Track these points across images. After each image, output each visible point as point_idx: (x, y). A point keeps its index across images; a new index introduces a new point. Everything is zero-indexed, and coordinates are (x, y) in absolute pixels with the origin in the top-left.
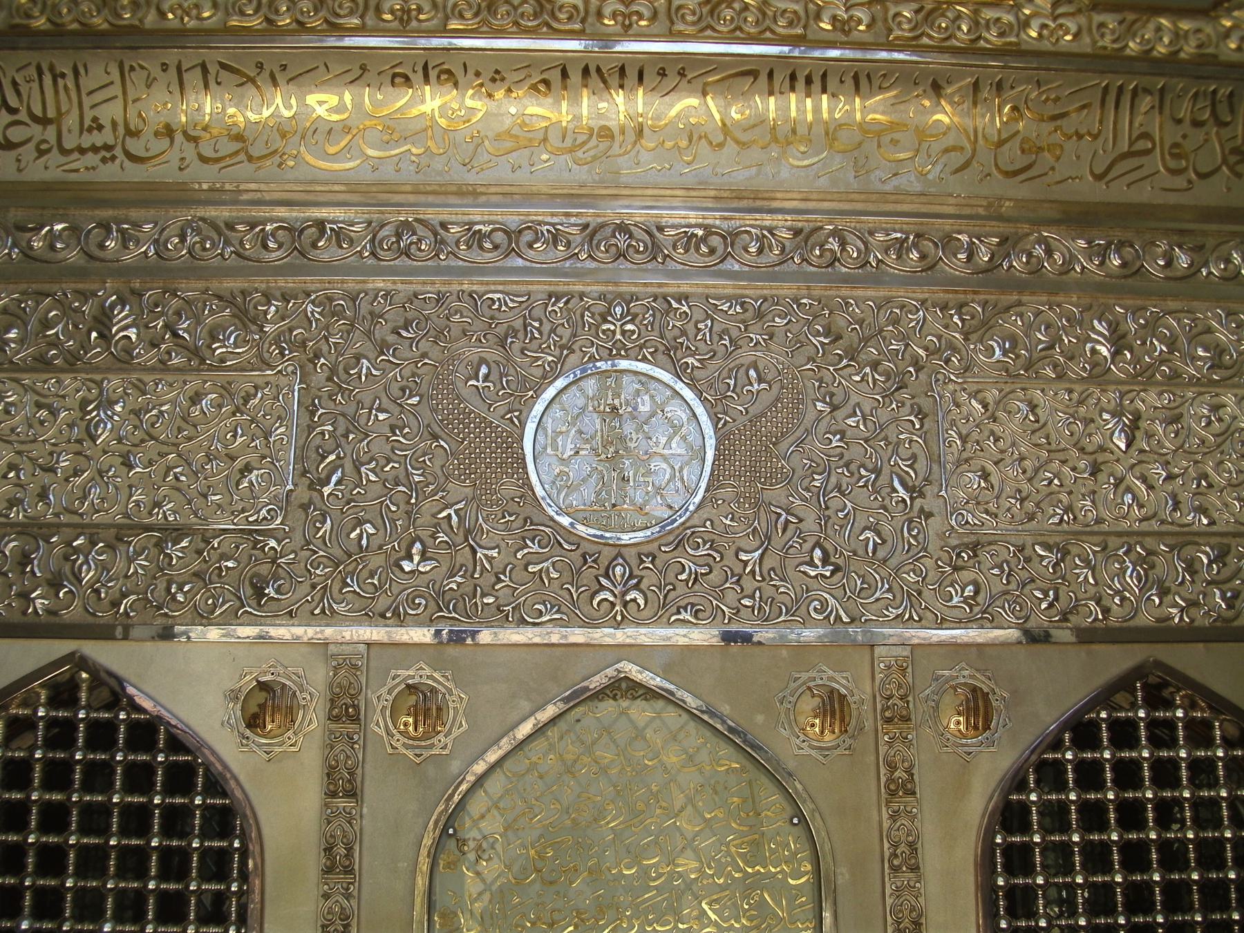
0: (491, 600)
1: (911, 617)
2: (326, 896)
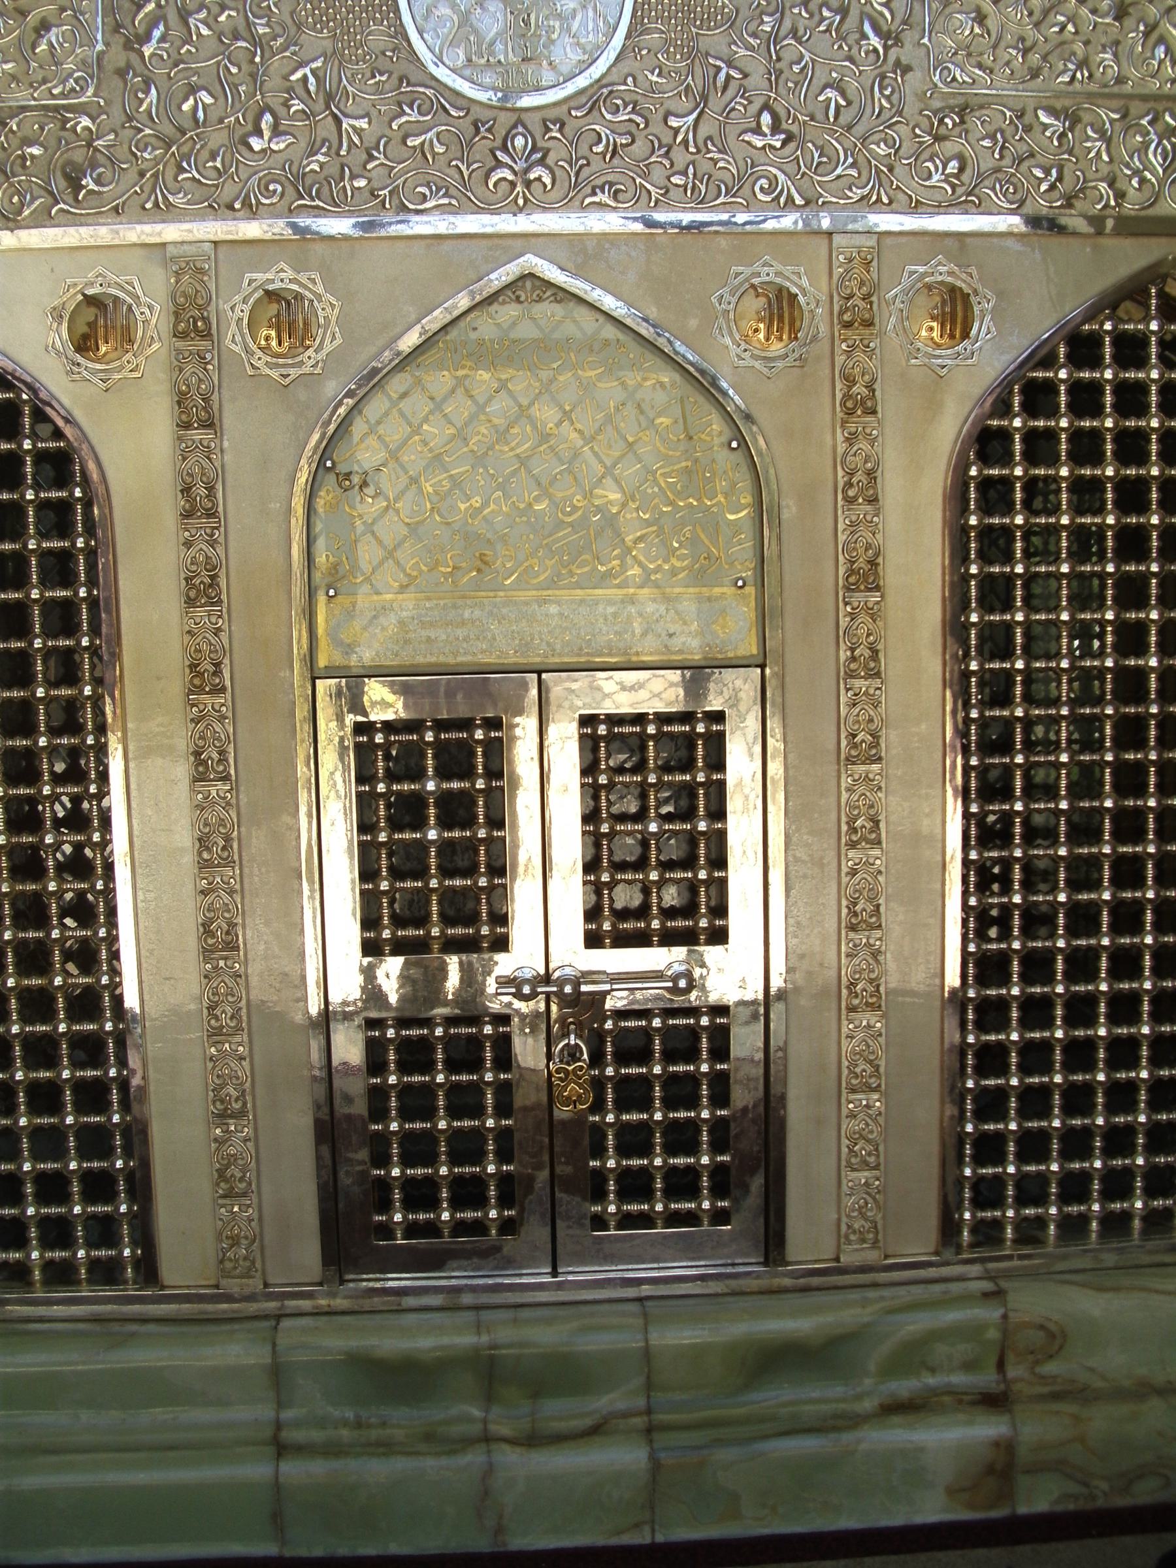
0: (362, 183)
1: (879, 200)
2: (188, 544)
